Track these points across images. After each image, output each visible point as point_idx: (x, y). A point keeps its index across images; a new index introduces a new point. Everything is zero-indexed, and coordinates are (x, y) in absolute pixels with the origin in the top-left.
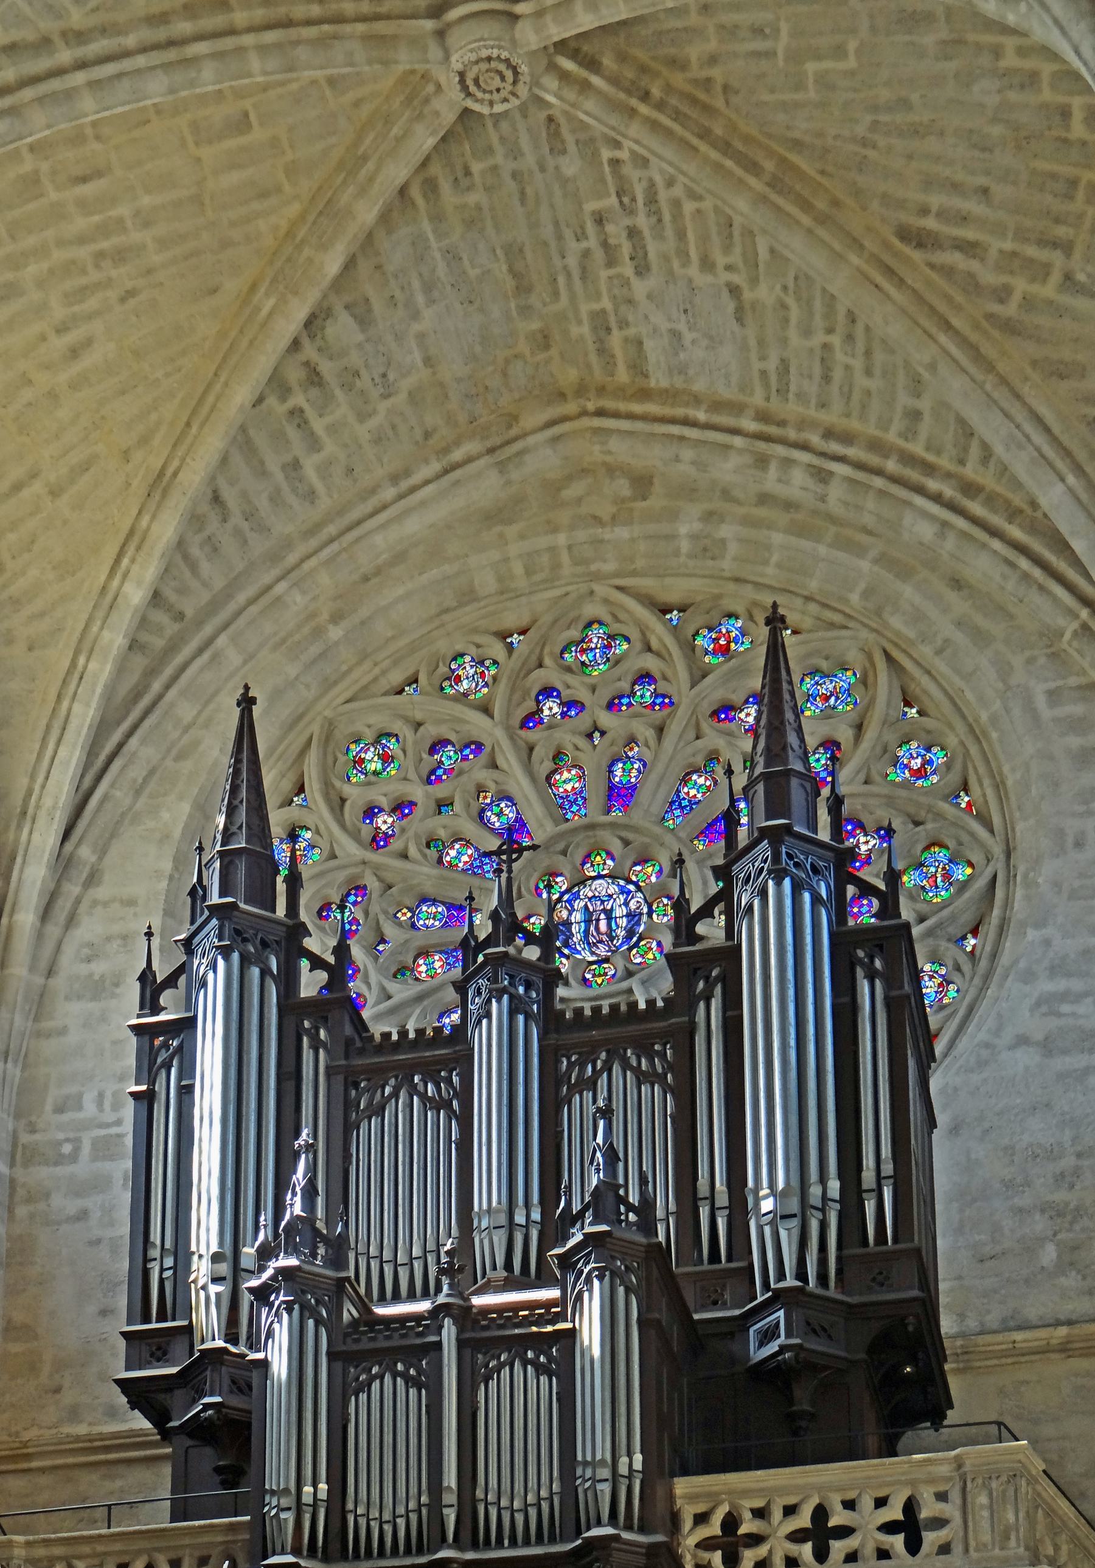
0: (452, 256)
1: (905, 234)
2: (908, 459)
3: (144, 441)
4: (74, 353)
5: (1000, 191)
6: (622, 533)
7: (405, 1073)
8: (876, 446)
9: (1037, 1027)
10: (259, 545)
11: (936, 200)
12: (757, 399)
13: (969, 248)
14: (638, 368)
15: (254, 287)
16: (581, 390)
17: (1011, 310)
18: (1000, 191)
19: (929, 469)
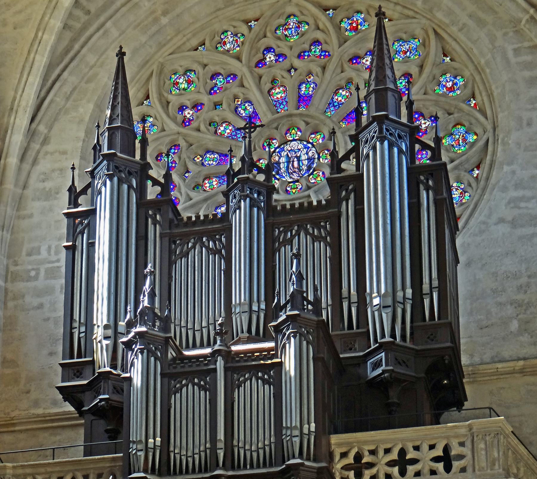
7: (199, 237)
9: (509, 214)
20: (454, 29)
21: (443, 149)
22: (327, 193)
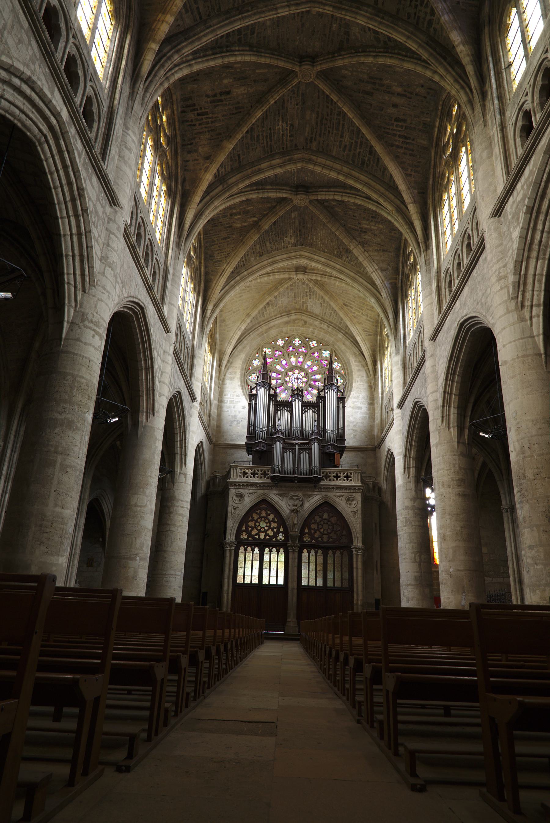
0: (288, 293)
1: (344, 304)
2: (339, 327)
3: (247, 309)
4: (240, 297)
5: (356, 302)
6: (303, 328)
7: (284, 406)
8: (335, 325)
9: (352, 405)
10: (257, 322)
11: (348, 301)
12: (321, 315)
13: (351, 307)
14: (307, 308)
15: (265, 294)
16: (299, 309)
17: (355, 315)
18: (356, 302)
19: (342, 329)
20: (340, 351)
21: (88, 423)
22: (315, 399)
